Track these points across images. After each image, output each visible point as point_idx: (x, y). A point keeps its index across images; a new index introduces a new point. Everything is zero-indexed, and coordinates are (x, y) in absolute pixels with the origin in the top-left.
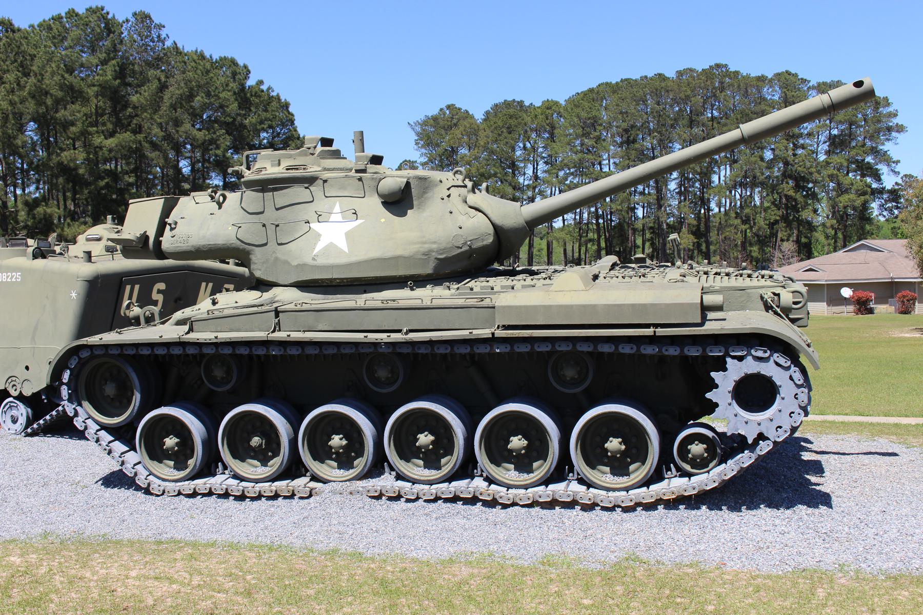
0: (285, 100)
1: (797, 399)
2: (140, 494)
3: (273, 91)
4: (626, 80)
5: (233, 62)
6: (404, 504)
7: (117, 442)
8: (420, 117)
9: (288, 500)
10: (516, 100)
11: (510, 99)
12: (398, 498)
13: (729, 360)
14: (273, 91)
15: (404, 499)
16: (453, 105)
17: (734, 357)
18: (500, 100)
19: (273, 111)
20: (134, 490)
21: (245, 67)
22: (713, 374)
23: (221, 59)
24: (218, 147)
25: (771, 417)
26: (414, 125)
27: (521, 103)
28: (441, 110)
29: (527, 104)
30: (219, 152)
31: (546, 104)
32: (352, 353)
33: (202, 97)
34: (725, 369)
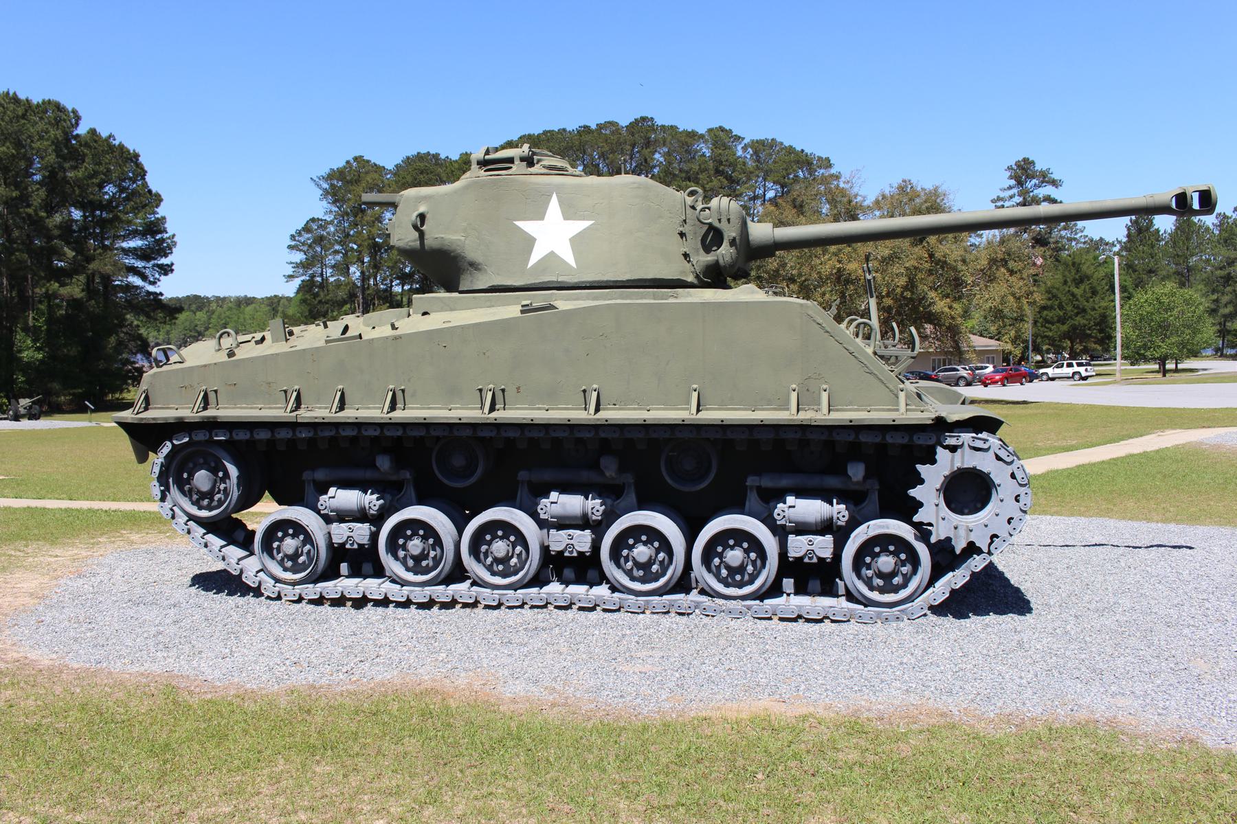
0: (134, 151)
1: (1017, 501)
2: (250, 598)
3: (114, 140)
4: (549, 131)
5: (58, 107)
6: (529, 611)
7: (210, 535)
8: (324, 171)
9: (468, 610)
10: (431, 153)
11: (423, 151)
12: (474, 605)
13: (939, 450)
14: (114, 140)
15: (460, 605)
16: (361, 157)
17: (946, 447)
18: (412, 152)
19: (106, 164)
20: (227, 595)
21: (74, 112)
22: (919, 467)
23: (44, 102)
24: (29, 206)
25: (986, 523)
26: (317, 180)
27: (436, 156)
28: (348, 162)
29: (443, 156)
30: (30, 211)
31: (465, 157)
32: (332, 436)
33: (8, 148)
34: (933, 462)
